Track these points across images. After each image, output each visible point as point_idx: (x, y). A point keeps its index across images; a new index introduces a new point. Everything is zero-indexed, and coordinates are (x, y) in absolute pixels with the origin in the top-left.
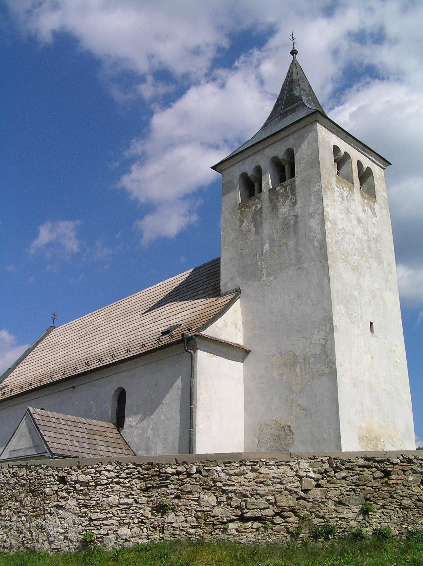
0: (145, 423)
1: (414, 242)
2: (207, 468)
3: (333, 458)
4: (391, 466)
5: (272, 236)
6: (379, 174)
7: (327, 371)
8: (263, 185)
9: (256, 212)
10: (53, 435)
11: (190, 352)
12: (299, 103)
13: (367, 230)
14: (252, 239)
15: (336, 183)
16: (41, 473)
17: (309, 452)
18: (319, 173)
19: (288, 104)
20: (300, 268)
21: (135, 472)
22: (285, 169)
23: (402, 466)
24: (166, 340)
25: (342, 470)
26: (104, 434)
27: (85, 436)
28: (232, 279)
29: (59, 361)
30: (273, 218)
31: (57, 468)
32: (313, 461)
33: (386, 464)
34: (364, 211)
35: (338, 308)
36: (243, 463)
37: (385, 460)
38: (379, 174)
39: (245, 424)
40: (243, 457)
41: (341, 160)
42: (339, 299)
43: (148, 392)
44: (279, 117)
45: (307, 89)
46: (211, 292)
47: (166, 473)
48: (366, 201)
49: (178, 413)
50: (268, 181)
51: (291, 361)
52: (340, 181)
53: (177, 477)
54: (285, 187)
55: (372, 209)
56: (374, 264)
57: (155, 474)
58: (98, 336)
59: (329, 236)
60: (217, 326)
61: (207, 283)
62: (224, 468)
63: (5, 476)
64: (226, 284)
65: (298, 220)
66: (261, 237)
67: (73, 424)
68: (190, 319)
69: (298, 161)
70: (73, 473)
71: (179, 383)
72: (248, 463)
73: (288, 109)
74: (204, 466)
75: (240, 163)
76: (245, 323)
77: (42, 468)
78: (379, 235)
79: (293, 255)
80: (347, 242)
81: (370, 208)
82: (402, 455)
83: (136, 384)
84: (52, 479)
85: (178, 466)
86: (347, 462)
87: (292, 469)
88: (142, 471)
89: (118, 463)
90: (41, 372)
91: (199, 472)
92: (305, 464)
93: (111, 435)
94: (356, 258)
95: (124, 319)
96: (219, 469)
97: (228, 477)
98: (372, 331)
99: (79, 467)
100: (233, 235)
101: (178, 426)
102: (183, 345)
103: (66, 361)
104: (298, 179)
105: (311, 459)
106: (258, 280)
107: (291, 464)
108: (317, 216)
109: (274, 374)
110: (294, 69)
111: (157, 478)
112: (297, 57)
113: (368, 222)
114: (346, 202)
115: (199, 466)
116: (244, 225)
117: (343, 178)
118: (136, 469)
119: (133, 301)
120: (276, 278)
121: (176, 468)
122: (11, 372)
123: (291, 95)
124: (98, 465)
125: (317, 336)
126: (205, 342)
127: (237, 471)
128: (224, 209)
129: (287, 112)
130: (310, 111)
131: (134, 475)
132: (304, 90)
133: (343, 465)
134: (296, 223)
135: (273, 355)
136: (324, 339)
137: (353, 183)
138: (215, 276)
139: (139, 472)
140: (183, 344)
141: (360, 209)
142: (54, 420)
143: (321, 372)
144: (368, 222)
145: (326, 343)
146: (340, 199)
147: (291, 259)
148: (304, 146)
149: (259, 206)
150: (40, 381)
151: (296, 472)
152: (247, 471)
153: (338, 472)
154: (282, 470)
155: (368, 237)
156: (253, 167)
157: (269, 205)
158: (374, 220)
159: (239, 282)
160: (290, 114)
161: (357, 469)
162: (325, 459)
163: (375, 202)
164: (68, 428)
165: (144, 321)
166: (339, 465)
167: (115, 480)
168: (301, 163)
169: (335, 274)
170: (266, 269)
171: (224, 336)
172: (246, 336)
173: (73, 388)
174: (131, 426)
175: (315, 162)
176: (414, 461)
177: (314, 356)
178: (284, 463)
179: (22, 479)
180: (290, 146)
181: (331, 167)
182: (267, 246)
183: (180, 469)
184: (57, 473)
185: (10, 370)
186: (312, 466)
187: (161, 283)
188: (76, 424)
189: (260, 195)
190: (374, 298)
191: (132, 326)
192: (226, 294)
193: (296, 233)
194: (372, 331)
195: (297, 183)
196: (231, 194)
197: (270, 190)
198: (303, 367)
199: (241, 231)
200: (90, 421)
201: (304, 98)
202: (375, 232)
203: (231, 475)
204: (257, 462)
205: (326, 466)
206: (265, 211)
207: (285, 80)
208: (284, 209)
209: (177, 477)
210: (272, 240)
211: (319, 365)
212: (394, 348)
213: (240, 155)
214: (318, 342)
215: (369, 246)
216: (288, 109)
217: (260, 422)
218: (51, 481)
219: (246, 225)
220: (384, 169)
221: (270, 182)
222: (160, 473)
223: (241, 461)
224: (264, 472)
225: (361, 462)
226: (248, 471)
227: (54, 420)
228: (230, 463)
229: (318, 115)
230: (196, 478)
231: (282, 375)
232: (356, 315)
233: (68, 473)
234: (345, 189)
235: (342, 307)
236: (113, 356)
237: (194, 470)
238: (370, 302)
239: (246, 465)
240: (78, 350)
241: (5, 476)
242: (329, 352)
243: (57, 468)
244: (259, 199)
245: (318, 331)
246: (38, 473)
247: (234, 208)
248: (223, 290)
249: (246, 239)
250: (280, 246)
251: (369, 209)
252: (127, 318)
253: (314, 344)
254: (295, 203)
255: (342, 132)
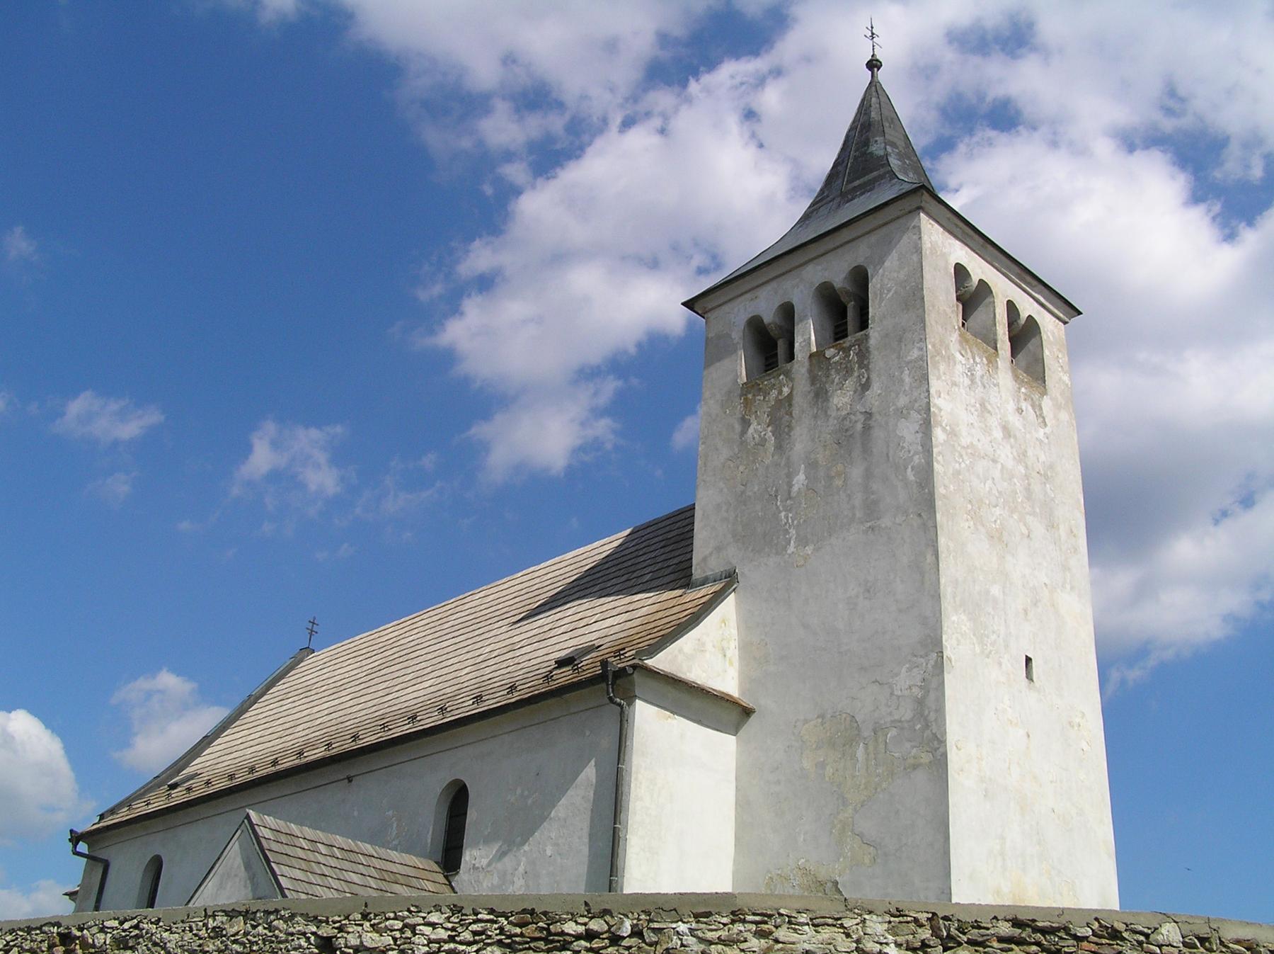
0: (508, 862)
1: (1125, 507)
2: (656, 925)
3: (940, 915)
4: (1072, 942)
5: (812, 456)
6: (1053, 334)
7: (926, 758)
8: (797, 345)
9: (779, 402)
10: (299, 874)
11: (619, 705)
12: (882, 171)
13: (1025, 454)
14: (767, 462)
15: (957, 346)
16: (277, 928)
17: (887, 900)
18: (923, 321)
19: (858, 172)
20: (872, 528)
21: (493, 931)
22: (846, 311)
23: (1097, 944)
24: (565, 676)
25: (960, 944)
26: (414, 882)
27: (372, 883)
28: (719, 549)
29: (318, 722)
30: (815, 417)
31: (316, 918)
32: (897, 920)
33: (1061, 938)
34: (1020, 411)
35: (954, 618)
36: (737, 916)
37: (1058, 929)
38: (1053, 334)
39: (735, 874)
40: (740, 903)
41: (972, 299)
42: (957, 599)
43: (519, 791)
44: (838, 200)
45: (901, 144)
46: (672, 577)
47: (563, 933)
48: (1023, 390)
49: (587, 840)
50: (808, 335)
51: (845, 734)
52: (967, 341)
53: (588, 945)
54: (846, 351)
55: (1038, 408)
56: (1039, 528)
57: (537, 934)
58: (409, 670)
59: (940, 458)
60: (681, 651)
61: (663, 557)
62: (694, 925)
63: (196, 935)
64: (705, 559)
65: (872, 423)
66: (788, 459)
67: (346, 855)
68: (622, 635)
69: (875, 293)
70: (350, 930)
71: (589, 773)
72: (750, 918)
73: (857, 183)
74: (650, 921)
75: (748, 296)
76: (745, 648)
77: (282, 918)
78: (1051, 467)
79: (858, 500)
80: (978, 477)
81: (1033, 406)
82: (1096, 919)
83: (490, 771)
84: (303, 942)
85: (591, 918)
86: (973, 927)
87: (848, 935)
88: (507, 928)
89: (456, 909)
90: (277, 745)
91: (637, 933)
92: (876, 925)
93: (430, 886)
94: (998, 511)
95: (471, 635)
96: (682, 927)
97: (702, 947)
98: (1029, 676)
99: (365, 916)
100: (725, 453)
101: (583, 869)
102: (604, 687)
103: (334, 722)
104: (875, 333)
105: (892, 916)
106: (777, 553)
107: (847, 923)
108: (914, 415)
109: (807, 764)
110: (874, 100)
111: (541, 944)
112: (881, 75)
113: (1028, 436)
114: (980, 389)
115: (639, 920)
116: (751, 430)
117: (975, 335)
118: (496, 922)
119: (491, 598)
120: (817, 550)
121: (585, 924)
122: (209, 744)
123: (864, 154)
124: (410, 912)
125: (906, 680)
126: (652, 684)
127: (723, 934)
128: (707, 394)
129: (855, 189)
130: (907, 187)
131: (490, 937)
132: (893, 145)
133: (964, 934)
134: (867, 428)
135: (806, 721)
136: (921, 687)
137: (996, 349)
138: (683, 543)
139: (501, 929)
140: (604, 685)
141: (1011, 406)
142: (304, 844)
143: (911, 761)
144: (1028, 436)
145: (924, 697)
146: (967, 382)
147: (853, 507)
148: (891, 262)
149: (786, 390)
150: (275, 763)
151: (858, 941)
152: (745, 934)
153: (951, 948)
154: (826, 936)
155: (1026, 467)
156: (777, 305)
157: (808, 388)
158: (1041, 433)
159: (733, 556)
160: (862, 194)
161: (995, 944)
162: (923, 917)
163: (1044, 393)
164: (333, 862)
165: (516, 639)
166: (954, 932)
167: (446, 947)
168: (881, 300)
169: (951, 545)
170: (797, 527)
171: (696, 674)
172: (746, 679)
173: (350, 779)
174: (475, 868)
175: (914, 298)
176: (1125, 935)
177: (897, 723)
178: (830, 921)
179: (235, 942)
180: (860, 261)
181: (948, 311)
182: (800, 479)
183: (596, 925)
184: (314, 929)
185: (207, 741)
186: (893, 930)
187: (557, 559)
188: (352, 856)
189: (789, 365)
190: (1035, 604)
191: (488, 649)
192: (704, 582)
193: (866, 450)
194: (1029, 676)
195: (872, 342)
196: (726, 363)
197: (811, 356)
198: (871, 748)
199: (743, 443)
200: (382, 852)
201: (894, 162)
202: (1042, 458)
203: (711, 943)
204: (770, 916)
205: (925, 934)
206: (800, 402)
207: (854, 122)
208: (841, 399)
209: (588, 945)
210: (812, 465)
211: (908, 745)
212: (1077, 720)
213: (747, 278)
214: (907, 693)
215: (1028, 489)
216: (857, 183)
217: (769, 871)
218: (300, 947)
219: (756, 430)
220: (1065, 323)
221: (813, 338)
222: (550, 933)
223: (733, 913)
224: (786, 939)
225: (1005, 929)
226: (749, 936)
227: (304, 844)
228: (708, 915)
229: (923, 195)
230: (630, 947)
231: (822, 765)
232: (993, 637)
233: (341, 929)
234: (978, 360)
235: (963, 617)
236: (442, 710)
237: (626, 929)
238: (1026, 611)
239: (744, 921)
240: (363, 700)
241: (196, 935)
242: (932, 716)
243: (316, 918)
244: (787, 374)
245: (909, 670)
246: (270, 928)
247: (730, 392)
248: (697, 573)
249: (754, 462)
250: (830, 478)
251: (1030, 408)
252: (477, 632)
253: (898, 697)
254: (866, 386)
255: (976, 237)
